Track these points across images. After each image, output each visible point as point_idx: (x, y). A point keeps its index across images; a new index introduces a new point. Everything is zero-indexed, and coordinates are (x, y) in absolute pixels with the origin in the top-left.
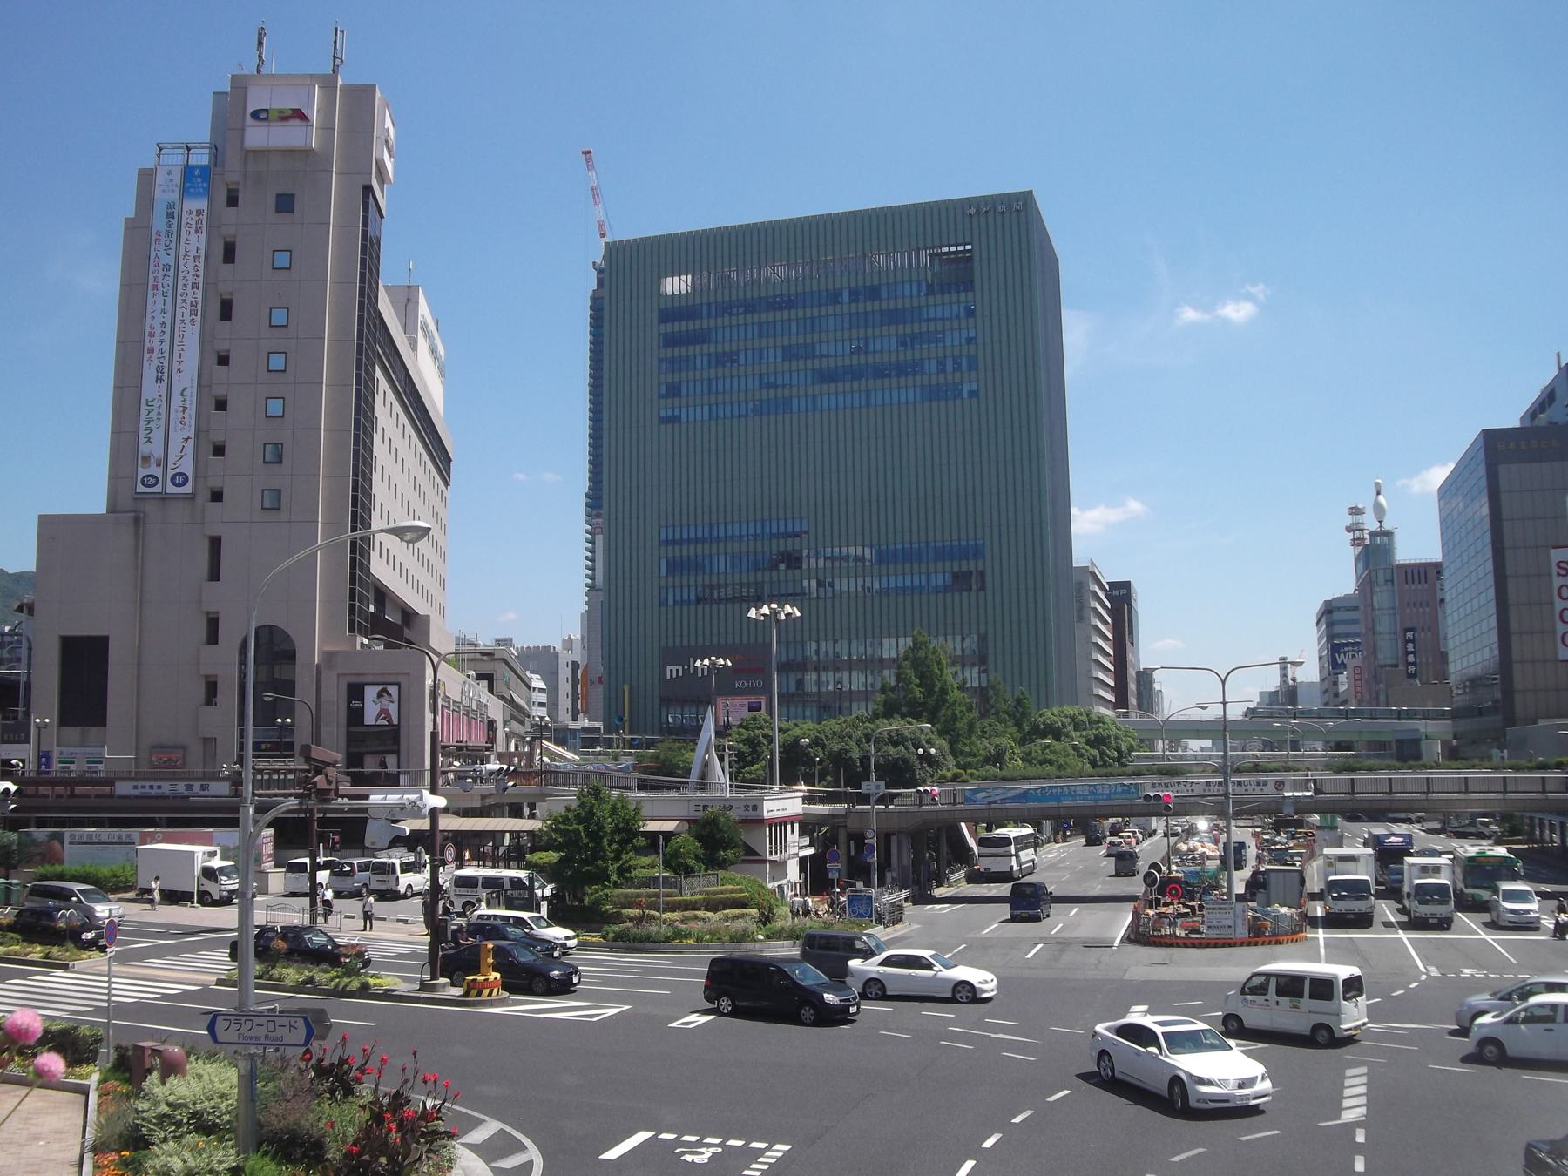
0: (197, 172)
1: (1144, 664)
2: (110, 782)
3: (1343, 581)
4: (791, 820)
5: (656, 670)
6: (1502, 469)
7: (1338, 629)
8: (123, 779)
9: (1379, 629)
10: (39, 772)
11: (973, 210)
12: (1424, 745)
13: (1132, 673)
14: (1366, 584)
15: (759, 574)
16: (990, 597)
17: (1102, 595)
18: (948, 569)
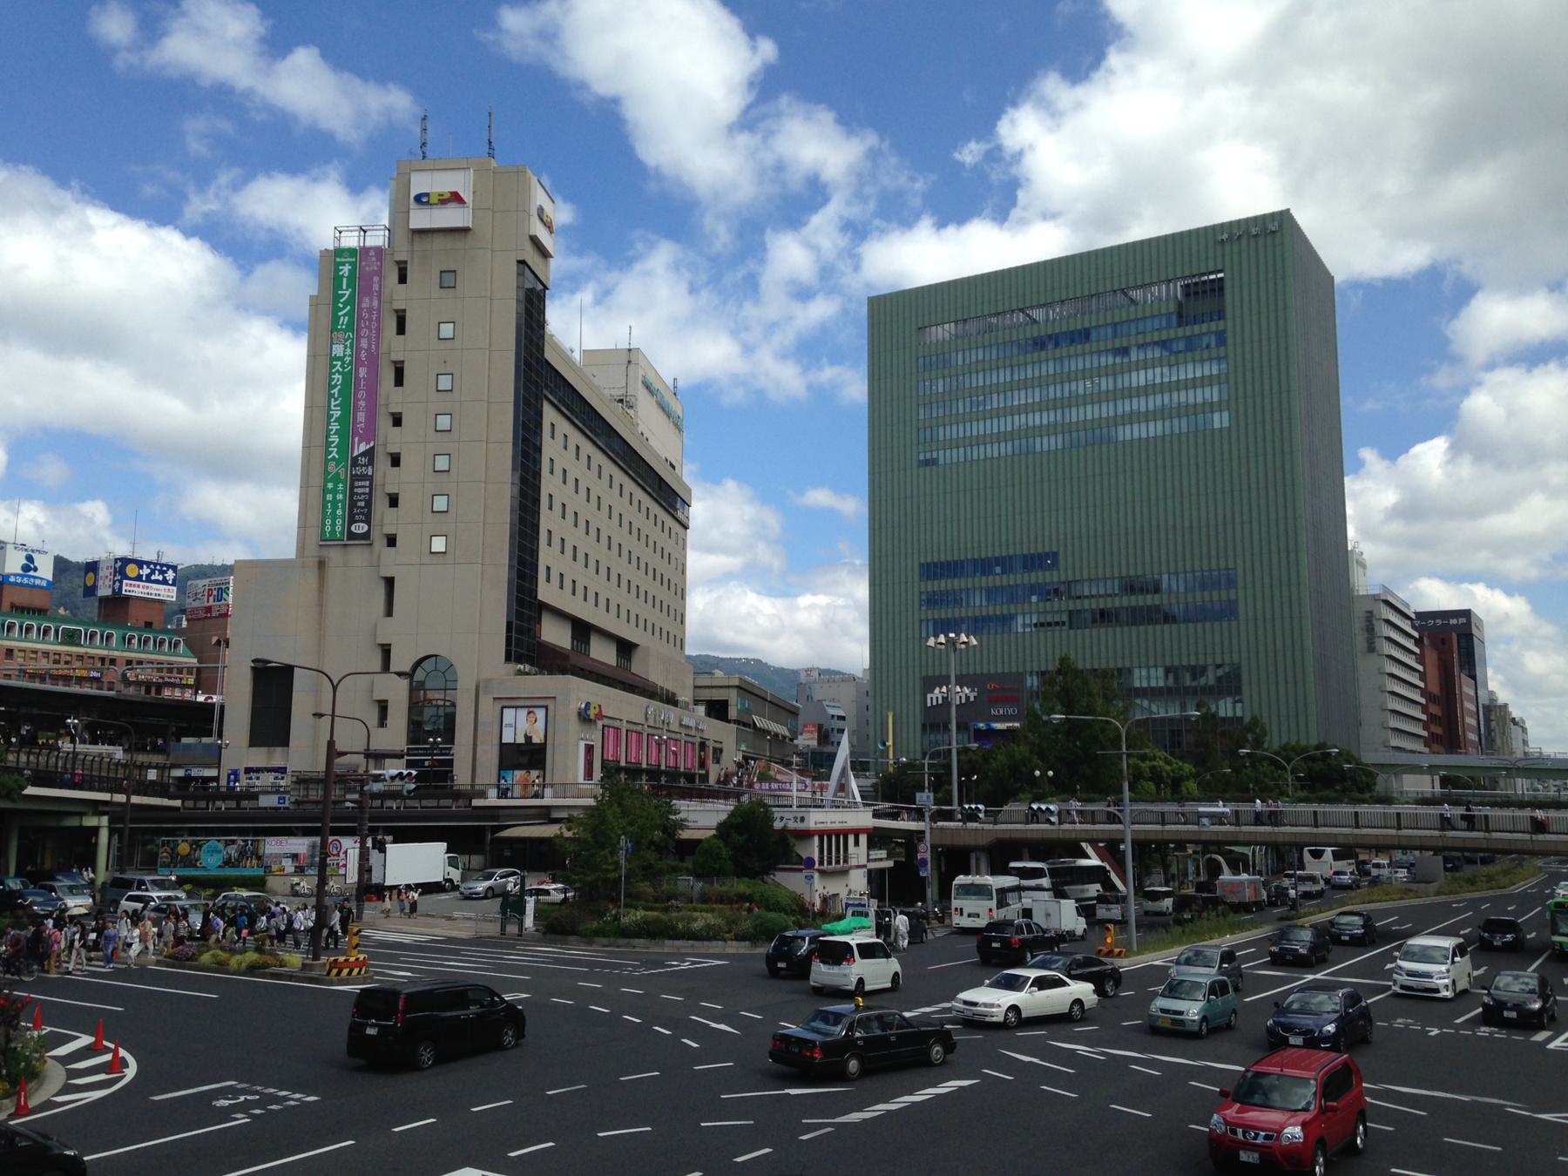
0: (372, 253)
2: (255, 797)
4: (856, 833)
5: (918, 698)
8: (267, 793)
10: (229, 788)
11: (1225, 236)
15: (1206, 593)
16: (1243, 627)
18: (1165, 597)
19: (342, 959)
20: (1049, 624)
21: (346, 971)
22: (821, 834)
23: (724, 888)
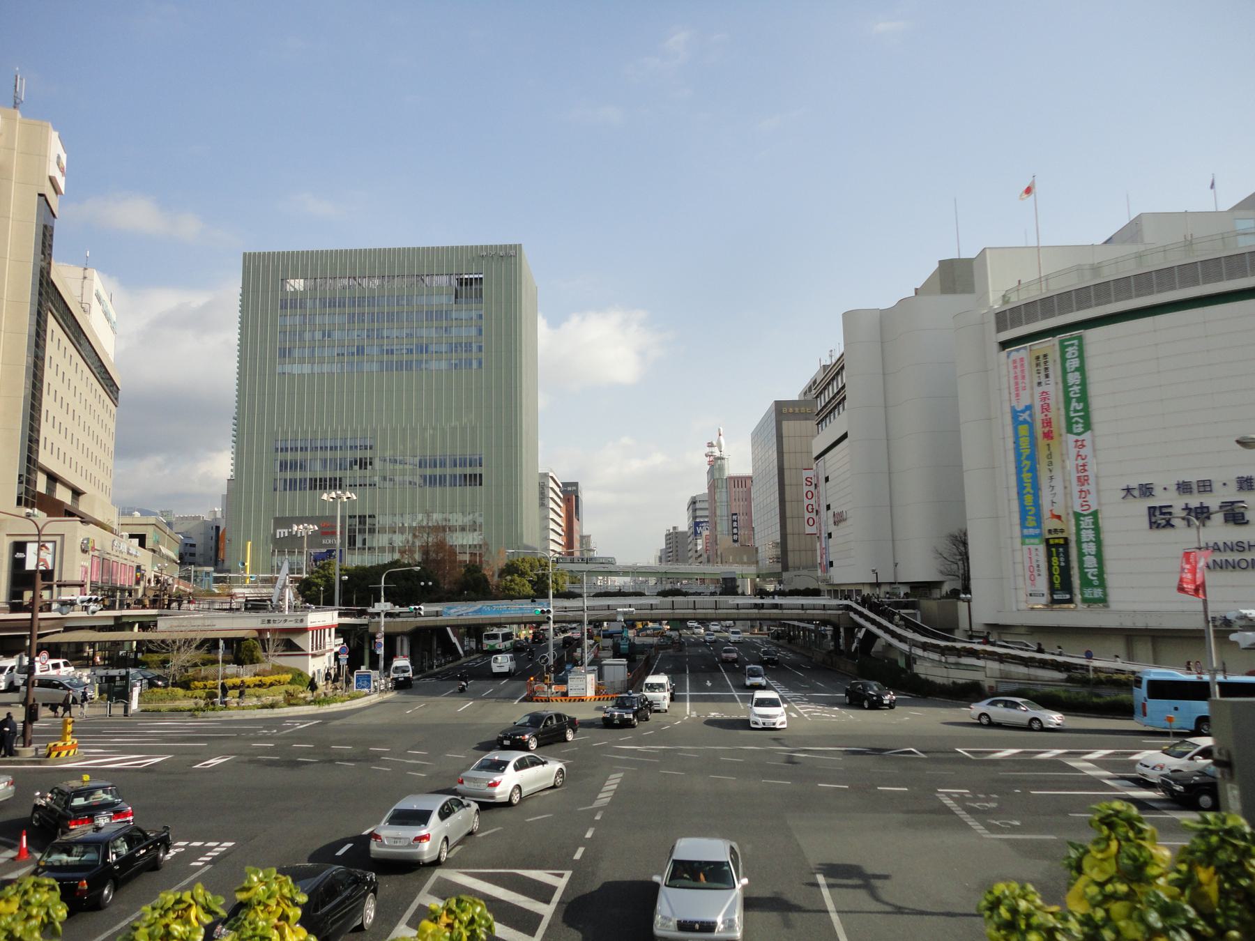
1: (585, 533)
3: (700, 487)
4: (330, 627)
6: (785, 424)
7: (699, 513)
9: (718, 512)
12: (739, 582)
13: (576, 537)
14: (713, 486)
17: (557, 490)
19: (60, 744)
20: (442, 479)
21: (64, 753)
22: (313, 629)
23: (1078, 690)
